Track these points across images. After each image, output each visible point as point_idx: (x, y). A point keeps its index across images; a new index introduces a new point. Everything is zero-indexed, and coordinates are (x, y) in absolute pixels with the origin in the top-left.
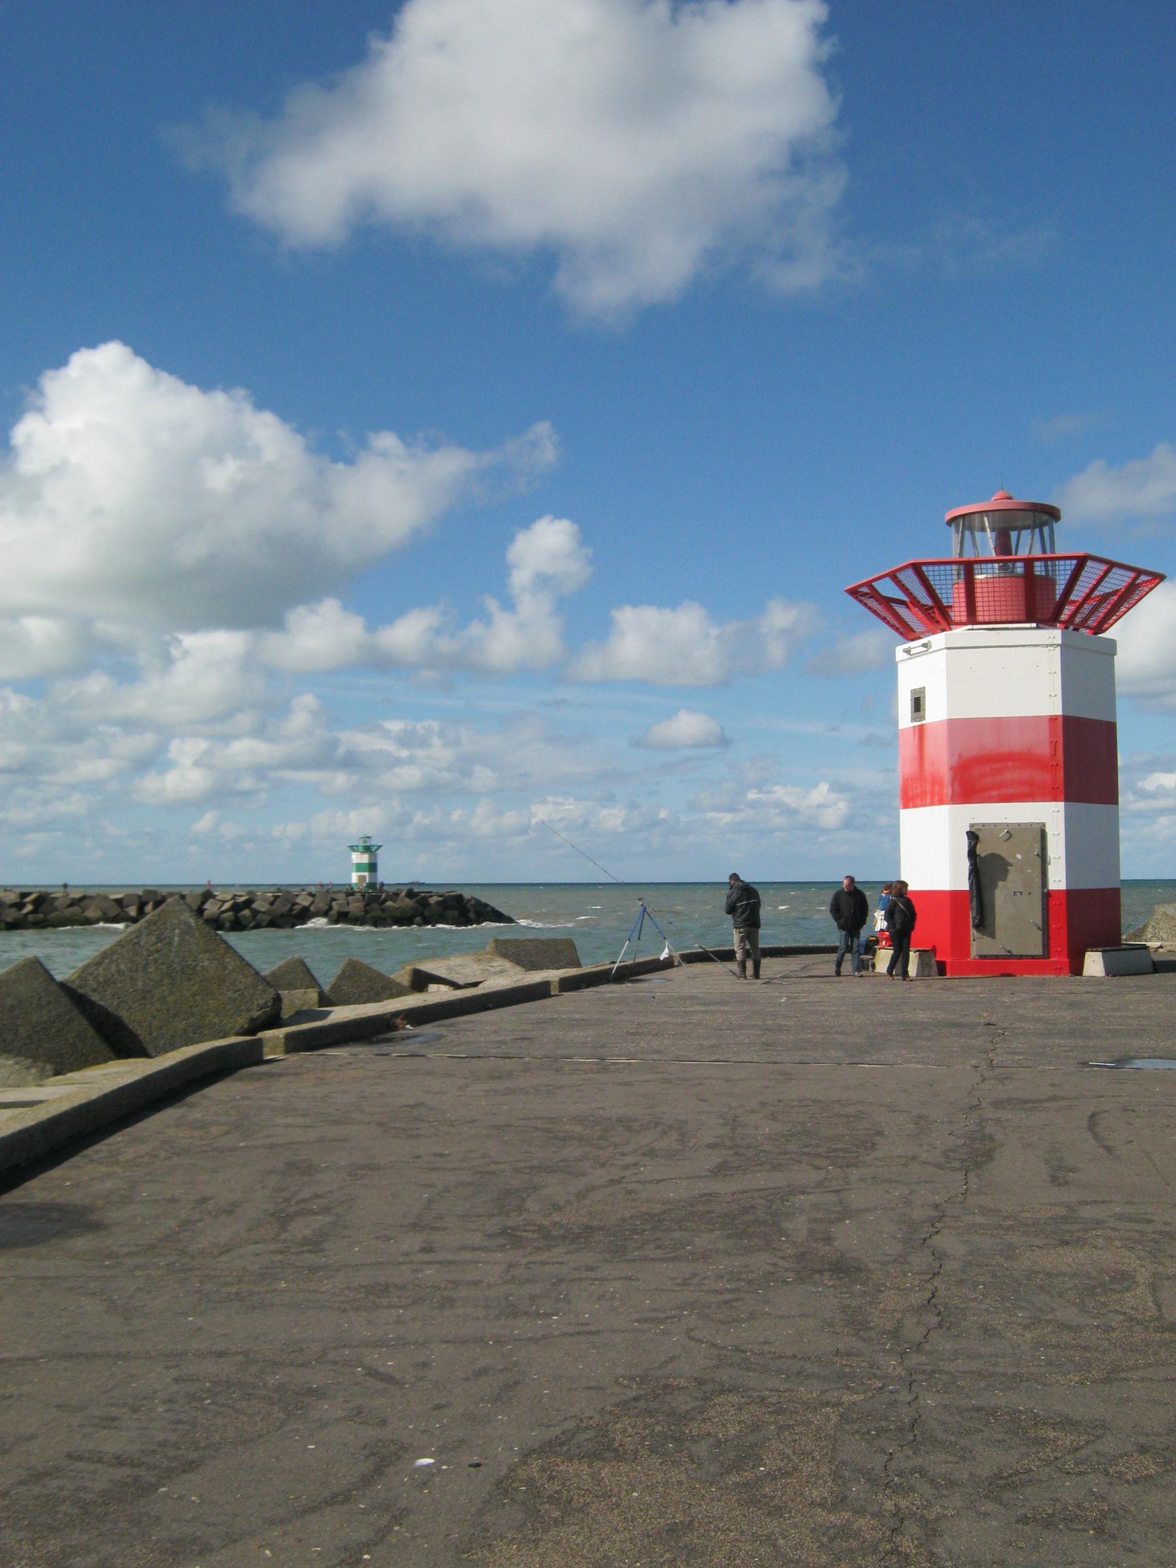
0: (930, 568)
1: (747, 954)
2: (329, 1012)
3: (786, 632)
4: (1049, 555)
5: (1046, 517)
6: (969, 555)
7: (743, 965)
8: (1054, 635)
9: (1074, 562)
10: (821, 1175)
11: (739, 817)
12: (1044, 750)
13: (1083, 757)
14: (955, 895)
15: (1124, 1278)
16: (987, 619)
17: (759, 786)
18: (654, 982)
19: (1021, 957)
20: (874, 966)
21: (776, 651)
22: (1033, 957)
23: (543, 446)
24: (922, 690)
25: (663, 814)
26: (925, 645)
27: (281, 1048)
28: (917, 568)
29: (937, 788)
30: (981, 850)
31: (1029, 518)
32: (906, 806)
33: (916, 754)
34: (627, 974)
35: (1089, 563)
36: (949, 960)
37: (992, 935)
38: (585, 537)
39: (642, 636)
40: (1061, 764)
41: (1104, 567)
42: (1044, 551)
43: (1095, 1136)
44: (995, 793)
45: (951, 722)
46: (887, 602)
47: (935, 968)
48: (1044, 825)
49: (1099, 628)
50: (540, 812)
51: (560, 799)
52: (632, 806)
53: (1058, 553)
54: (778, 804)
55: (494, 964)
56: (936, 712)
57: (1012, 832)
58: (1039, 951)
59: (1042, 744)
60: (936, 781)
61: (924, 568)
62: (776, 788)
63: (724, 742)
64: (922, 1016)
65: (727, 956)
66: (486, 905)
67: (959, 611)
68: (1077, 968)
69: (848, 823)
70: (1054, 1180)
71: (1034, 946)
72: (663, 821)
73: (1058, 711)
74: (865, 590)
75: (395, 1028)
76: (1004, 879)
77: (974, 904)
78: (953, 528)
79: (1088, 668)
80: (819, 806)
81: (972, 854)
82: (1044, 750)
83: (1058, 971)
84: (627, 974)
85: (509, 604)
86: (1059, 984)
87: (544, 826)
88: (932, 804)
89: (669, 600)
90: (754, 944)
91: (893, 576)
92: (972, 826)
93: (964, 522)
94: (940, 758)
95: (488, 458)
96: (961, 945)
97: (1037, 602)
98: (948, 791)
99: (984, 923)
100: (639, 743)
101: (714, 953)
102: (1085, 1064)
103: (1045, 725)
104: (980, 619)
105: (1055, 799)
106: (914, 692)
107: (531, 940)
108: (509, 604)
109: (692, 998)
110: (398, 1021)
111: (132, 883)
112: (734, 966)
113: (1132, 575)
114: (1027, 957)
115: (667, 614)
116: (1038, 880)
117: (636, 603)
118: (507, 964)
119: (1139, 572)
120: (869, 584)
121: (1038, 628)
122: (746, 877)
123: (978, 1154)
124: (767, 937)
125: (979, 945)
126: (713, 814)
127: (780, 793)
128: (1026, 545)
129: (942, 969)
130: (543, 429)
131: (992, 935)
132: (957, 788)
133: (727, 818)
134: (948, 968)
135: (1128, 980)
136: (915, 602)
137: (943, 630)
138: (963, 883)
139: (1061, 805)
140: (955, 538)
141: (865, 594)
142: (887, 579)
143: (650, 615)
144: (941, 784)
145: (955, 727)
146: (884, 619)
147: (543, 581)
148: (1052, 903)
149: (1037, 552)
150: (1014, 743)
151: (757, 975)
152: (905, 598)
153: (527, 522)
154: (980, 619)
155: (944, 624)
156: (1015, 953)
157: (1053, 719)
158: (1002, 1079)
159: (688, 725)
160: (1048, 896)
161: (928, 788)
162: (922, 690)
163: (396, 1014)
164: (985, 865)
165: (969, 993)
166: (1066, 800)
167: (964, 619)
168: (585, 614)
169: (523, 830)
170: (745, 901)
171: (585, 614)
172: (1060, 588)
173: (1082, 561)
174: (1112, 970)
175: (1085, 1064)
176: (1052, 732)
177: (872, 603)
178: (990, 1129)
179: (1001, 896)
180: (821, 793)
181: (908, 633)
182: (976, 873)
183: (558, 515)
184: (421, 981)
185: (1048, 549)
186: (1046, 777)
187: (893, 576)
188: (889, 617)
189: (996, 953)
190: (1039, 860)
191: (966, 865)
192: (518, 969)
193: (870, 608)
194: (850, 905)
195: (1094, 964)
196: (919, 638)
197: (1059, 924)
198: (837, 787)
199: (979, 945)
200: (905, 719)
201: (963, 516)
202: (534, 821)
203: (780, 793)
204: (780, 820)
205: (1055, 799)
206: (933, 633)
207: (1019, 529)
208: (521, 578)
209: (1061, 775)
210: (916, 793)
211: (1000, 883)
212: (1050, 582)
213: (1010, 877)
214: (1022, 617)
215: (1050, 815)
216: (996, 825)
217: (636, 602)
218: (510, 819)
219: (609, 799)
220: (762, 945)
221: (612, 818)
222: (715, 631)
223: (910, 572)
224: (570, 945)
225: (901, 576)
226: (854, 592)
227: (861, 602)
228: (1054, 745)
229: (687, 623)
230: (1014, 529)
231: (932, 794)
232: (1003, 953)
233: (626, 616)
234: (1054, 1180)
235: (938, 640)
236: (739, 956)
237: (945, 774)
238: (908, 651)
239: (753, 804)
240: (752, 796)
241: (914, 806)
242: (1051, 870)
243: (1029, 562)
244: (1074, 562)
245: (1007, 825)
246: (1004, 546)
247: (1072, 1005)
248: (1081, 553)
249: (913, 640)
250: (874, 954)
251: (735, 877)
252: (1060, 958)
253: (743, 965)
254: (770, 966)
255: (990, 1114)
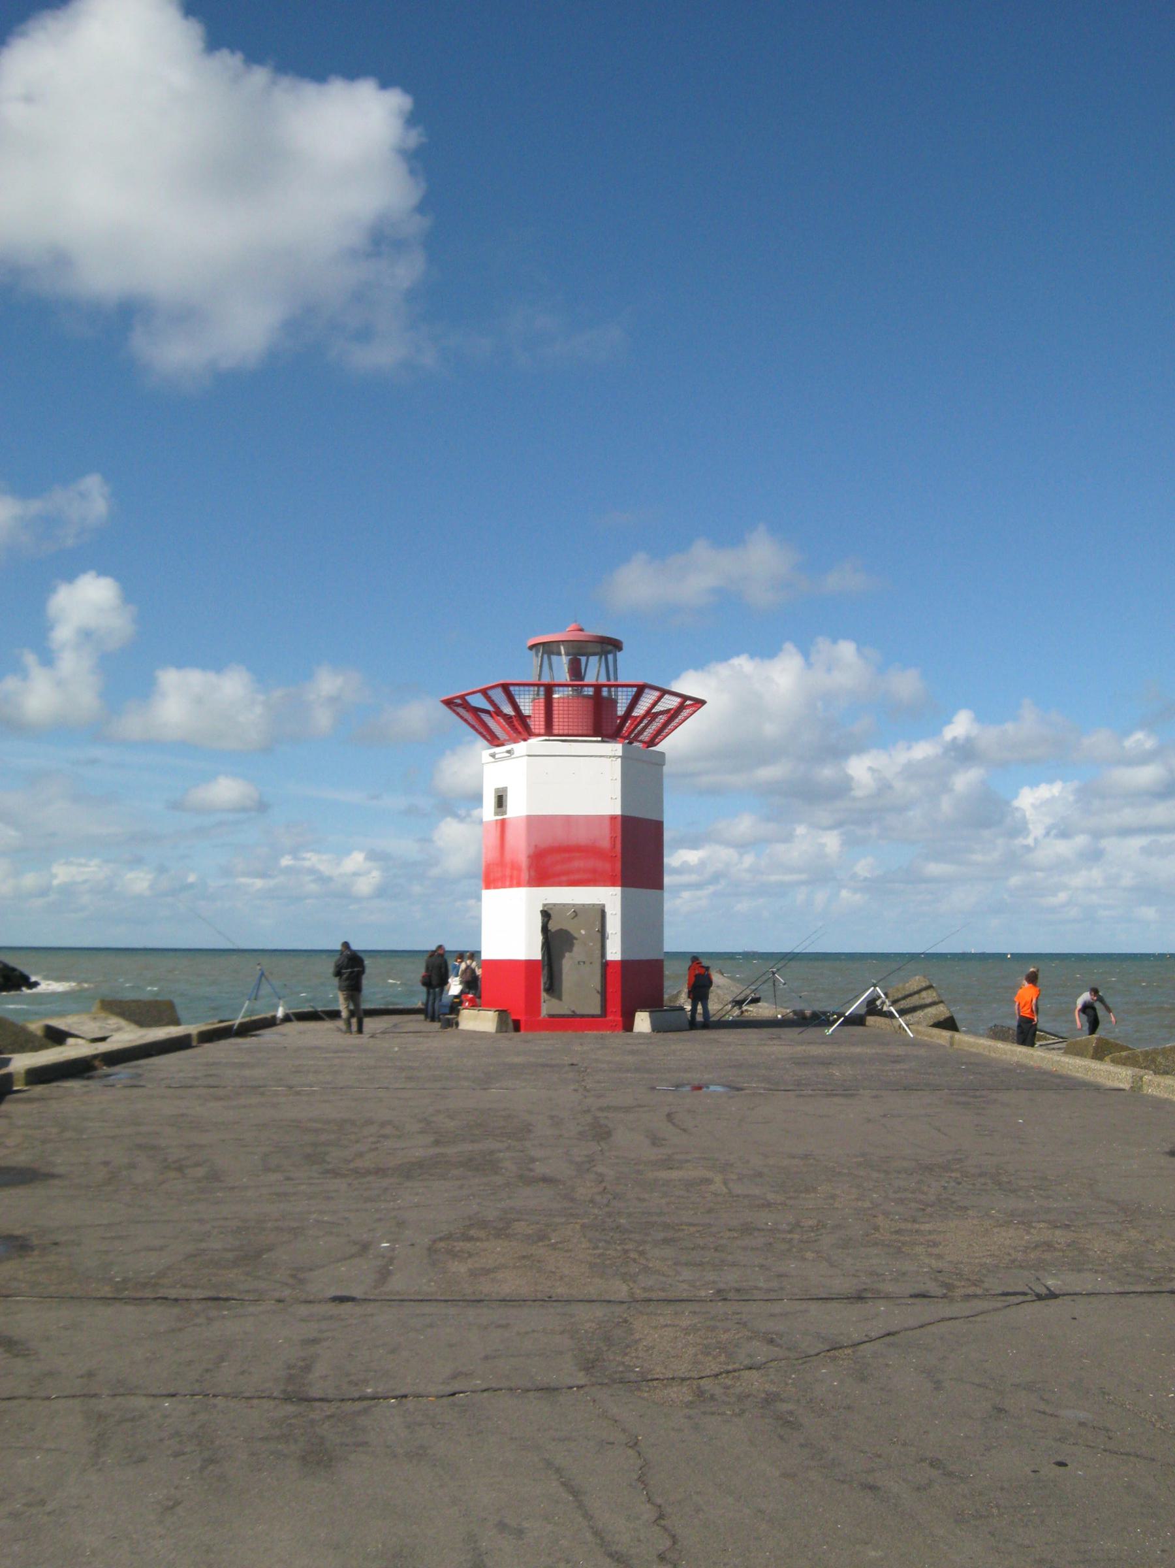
0: (517, 688)
1: (352, 1014)
2: (9, 1060)
3: (333, 700)
4: (613, 682)
5: (610, 648)
6: (546, 679)
7: (349, 1024)
8: (616, 748)
9: (635, 689)
10: (506, 1144)
11: (272, 883)
12: (605, 843)
13: (635, 851)
14: (529, 964)
15: (709, 1181)
16: (561, 732)
17: (294, 852)
18: (268, 1036)
19: (583, 1016)
20: (457, 1024)
21: (323, 719)
22: (593, 1016)
23: (92, 500)
24: (505, 789)
25: (191, 878)
26: (508, 752)
27: (22, 1081)
28: (505, 687)
29: (515, 873)
30: (553, 926)
31: (598, 649)
32: (488, 887)
33: (498, 842)
34: (246, 1030)
35: (647, 691)
36: (522, 1018)
37: (560, 998)
38: (129, 594)
39: (181, 698)
40: (619, 855)
41: (657, 694)
42: (609, 679)
43: (674, 1124)
44: (564, 878)
45: (530, 819)
46: (475, 711)
47: (511, 1025)
48: (604, 906)
49: (652, 742)
50: (62, 873)
51: (83, 861)
52: (162, 869)
53: (620, 681)
54: (312, 871)
55: (110, 1022)
56: (516, 809)
57: (578, 911)
58: (598, 1011)
59: (604, 838)
60: (515, 867)
61: (512, 688)
62: (308, 855)
63: (262, 807)
64: (518, 1060)
65: (334, 1015)
66: (14, 970)
67: (537, 724)
68: (628, 1026)
69: (381, 892)
70: (654, 1144)
71: (593, 1006)
72: (191, 886)
73: (618, 811)
74: (459, 701)
75: (94, 1068)
76: (571, 951)
77: (545, 972)
78: (533, 652)
79: (642, 776)
80: (356, 874)
81: (545, 929)
82: (605, 843)
83: (612, 1028)
84: (246, 1030)
85: (48, 659)
86: (617, 1038)
87: (68, 890)
88: (511, 886)
89: (215, 664)
90: (357, 1004)
91: (484, 692)
92: (545, 905)
93: (548, 649)
94: (519, 847)
95: (35, 506)
96: (533, 1005)
97: (603, 719)
98: (525, 876)
99: (553, 988)
100: (176, 806)
101: (324, 1012)
102: (653, 1088)
103: (607, 822)
104: (556, 732)
105: (613, 884)
106: (497, 790)
107: (134, 1001)
108: (48, 659)
109: (317, 1048)
110: (97, 1063)
111: (150, 945)
112: (341, 1024)
113: (679, 700)
114: (588, 1016)
115: (212, 677)
116: (598, 953)
117: (180, 665)
118: (123, 1023)
119: (685, 698)
120: (462, 697)
121: (602, 741)
122: (355, 946)
123: (602, 1134)
124: (371, 996)
125: (548, 1006)
126: (243, 880)
127: (312, 859)
128: (594, 671)
129: (517, 1027)
130: (93, 483)
131: (560, 998)
132: (533, 873)
133: (259, 883)
134: (522, 1025)
135: (670, 1035)
136: (499, 712)
137: (525, 740)
138: (537, 954)
139: (617, 890)
140: (536, 661)
141: (459, 705)
142: (479, 695)
143: (195, 678)
144: (519, 869)
145: (534, 822)
146: (473, 727)
147: (86, 635)
148: (610, 970)
149: (603, 680)
150: (581, 837)
151: (360, 1031)
152: (490, 708)
153: (70, 577)
154: (556, 732)
155: (525, 735)
156: (578, 1012)
157: (613, 818)
158: (599, 1096)
159: (226, 790)
160: (606, 965)
161: (508, 872)
162: (505, 789)
163: (95, 1057)
164: (555, 939)
165: (544, 1042)
166: (622, 886)
167: (542, 731)
168: (126, 672)
169: (44, 892)
170: (351, 967)
171: (126, 672)
172: (621, 711)
173: (641, 689)
174: (657, 1027)
175: (653, 1088)
176: (613, 829)
177: (461, 710)
178: (602, 1121)
179: (568, 965)
180: (356, 860)
181: (494, 740)
182: (547, 946)
183: (102, 572)
184: (57, 1037)
185: (612, 677)
186: (607, 866)
187: (484, 692)
188: (482, 730)
189: (562, 1012)
190: (599, 935)
191: (539, 938)
192: (133, 1027)
193: (461, 717)
194: (437, 968)
195: (643, 1022)
196: (502, 745)
197: (615, 988)
198: (373, 856)
199: (548, 1006)
200: (488, 811)
201: (543, 644)
202: (55, 882)
203: (312, 859)
204: (313, 887)
205: (613, 885)
206: (516, 742)
207: (588, 655)
208: (63, 633)
209: (619, 865)
210: (497, 875)
211: (567, 954)
212: (613, 703)
213: (575, 949)
214: (591, 732)
215: (609, 897)
216: (564, 905)
217: (180, 664)
218: (30, 880)
219: (137, 862)
220: (366, 1006)
221: (139, 881)
222: (261, 698)
223: (500, 690)
224: (171, 1005)
225: (491, 693)
226: (449, 703)
227: (454, 711)
228: (613, 839)
229: (233, 686)
230: (583, 655)
231: (512, 877)
232: (569, 1013)
233: (170, 678)
234: (654, 1144)
235: (521, 747)
236: (344, 1014)
237: (522, 859)
238: (493, 756)
239: (289, 870)
240: (286, 861)
241: (495, 888)
242: (609, 943)
243: (598, 688)
244: (635, 689)
245: (574, 905)
246: (576, 671)
247: (632, 1052)
248: (640, 681)
249: (498, 746)
250: (457, 1013)
251: (346, 945)
252: (615, 1017)
253: (349, 1024)
254: (370, 1024)
255: (599, 1114)
